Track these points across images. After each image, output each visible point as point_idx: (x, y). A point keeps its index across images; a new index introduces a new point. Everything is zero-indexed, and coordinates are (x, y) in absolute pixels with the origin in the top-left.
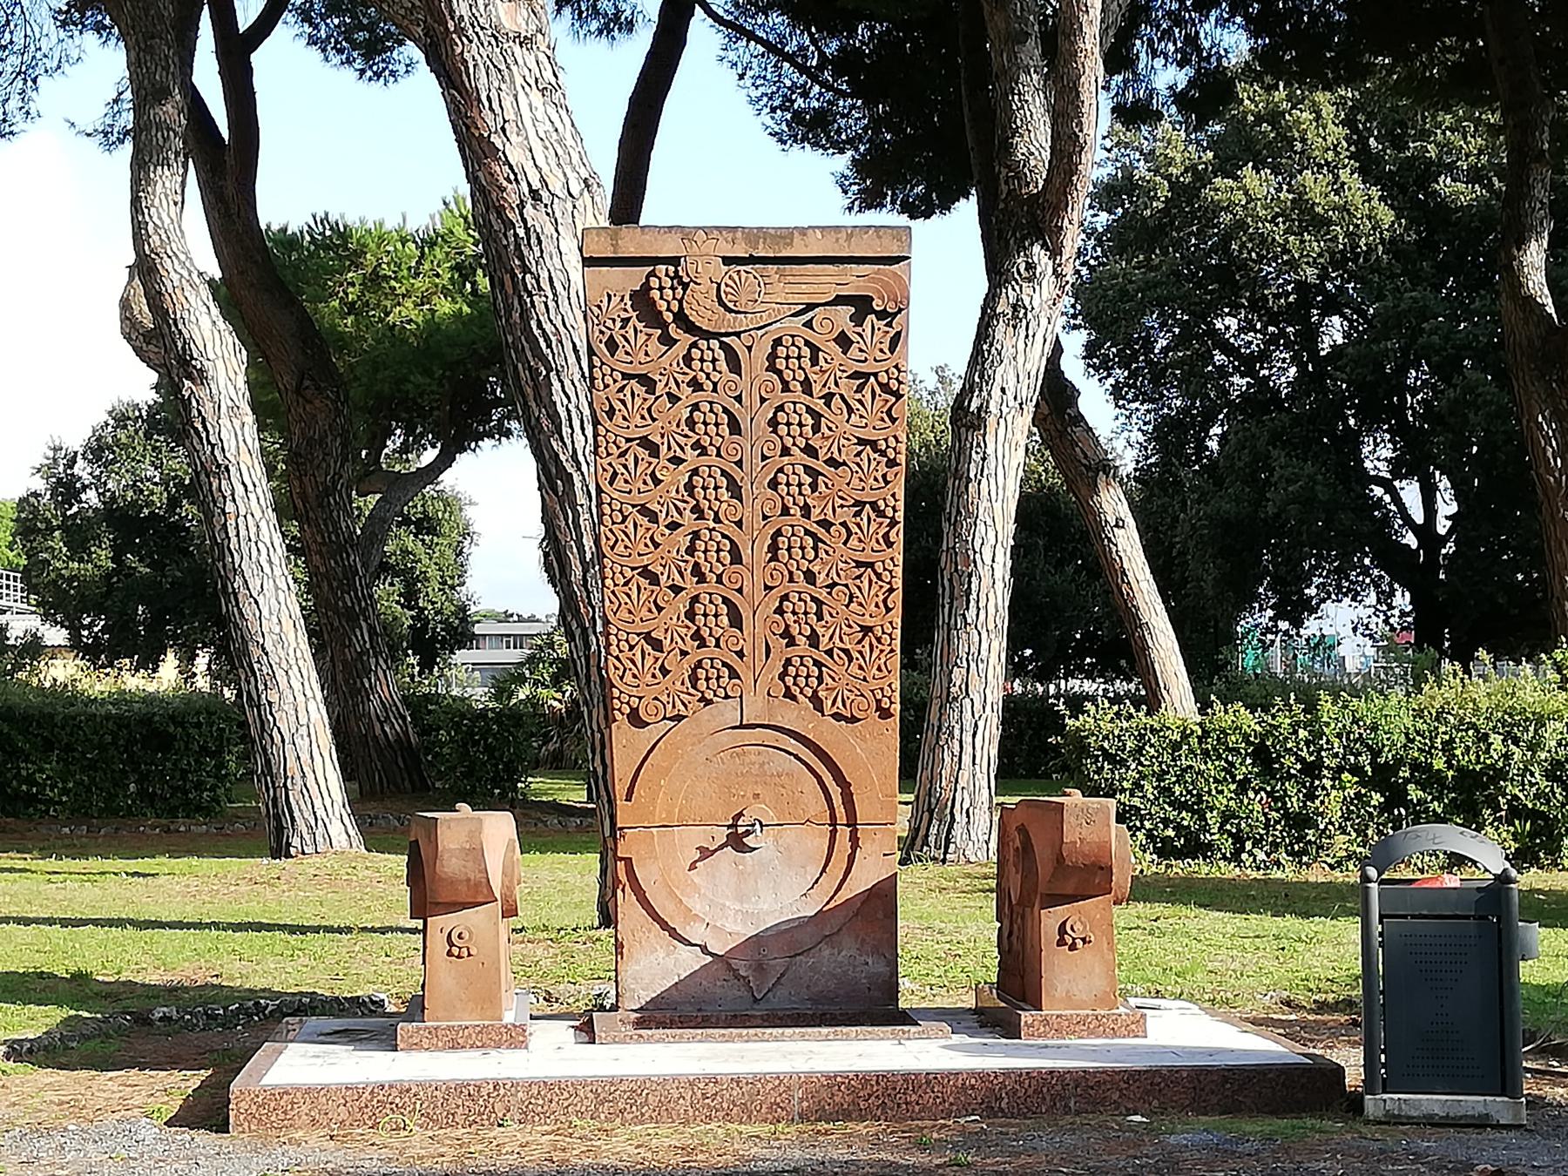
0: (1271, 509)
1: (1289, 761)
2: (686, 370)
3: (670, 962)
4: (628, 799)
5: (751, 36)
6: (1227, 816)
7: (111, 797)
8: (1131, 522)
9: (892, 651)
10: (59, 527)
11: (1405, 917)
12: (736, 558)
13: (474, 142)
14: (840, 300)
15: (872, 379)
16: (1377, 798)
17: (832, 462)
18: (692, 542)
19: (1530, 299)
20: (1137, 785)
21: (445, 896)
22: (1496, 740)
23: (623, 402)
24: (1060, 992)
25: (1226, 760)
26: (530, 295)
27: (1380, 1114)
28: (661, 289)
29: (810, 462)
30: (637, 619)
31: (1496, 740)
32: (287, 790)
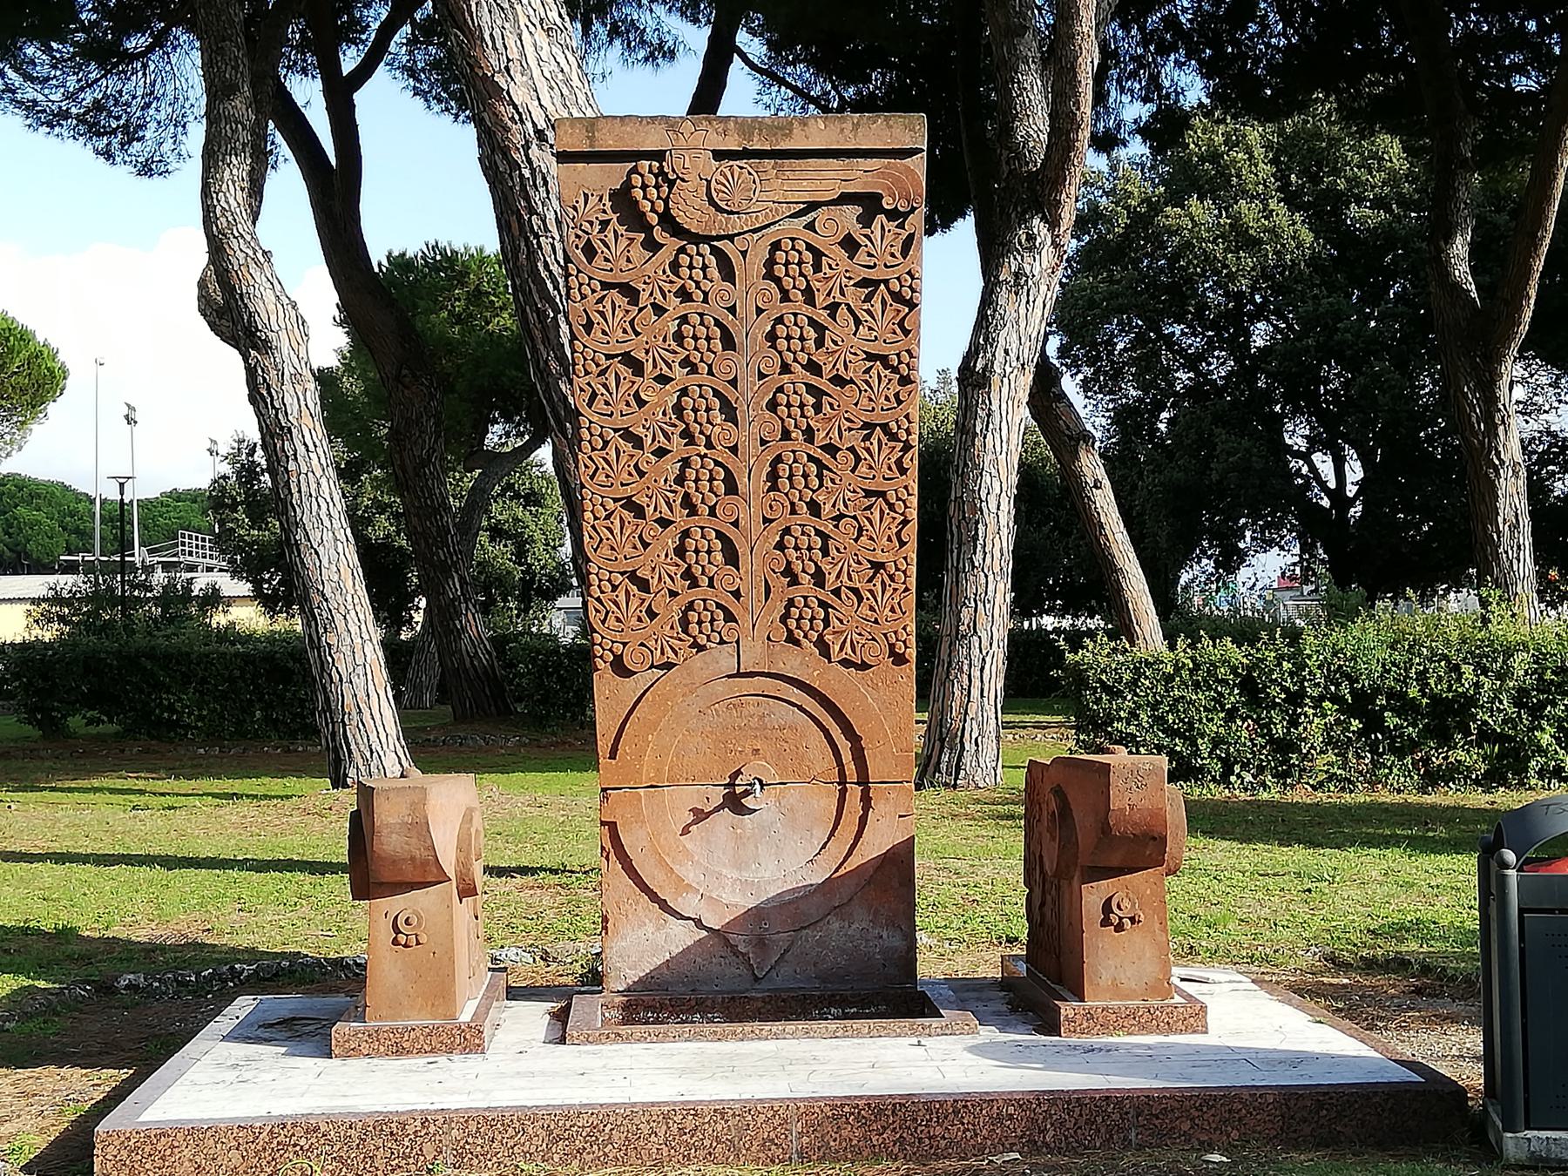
0: (1215, 477)
1: (1274, 691)
2: (675, 279)
4: (613, 756)
5: (782, 82)
6: (1217, 742)
7: (240, 723)
8: (1106, 483)
9: (907, 590)
10: (242, 503)
11: (1551, 911)
12: (731, 488)
14: (845, 199)
16: (1356, 724)
17: (838, 381)
18: (683, 470)
19: (1457, 289)
20: (1133, 714)
21: (387, 875)
23: (602, 314)
24: (1105, 978)
25: (1216, 691)
26: (537, 236)
27: (1523, 1156)
29: (813, 380)
31: (1467, 670)
32: (344, 725)
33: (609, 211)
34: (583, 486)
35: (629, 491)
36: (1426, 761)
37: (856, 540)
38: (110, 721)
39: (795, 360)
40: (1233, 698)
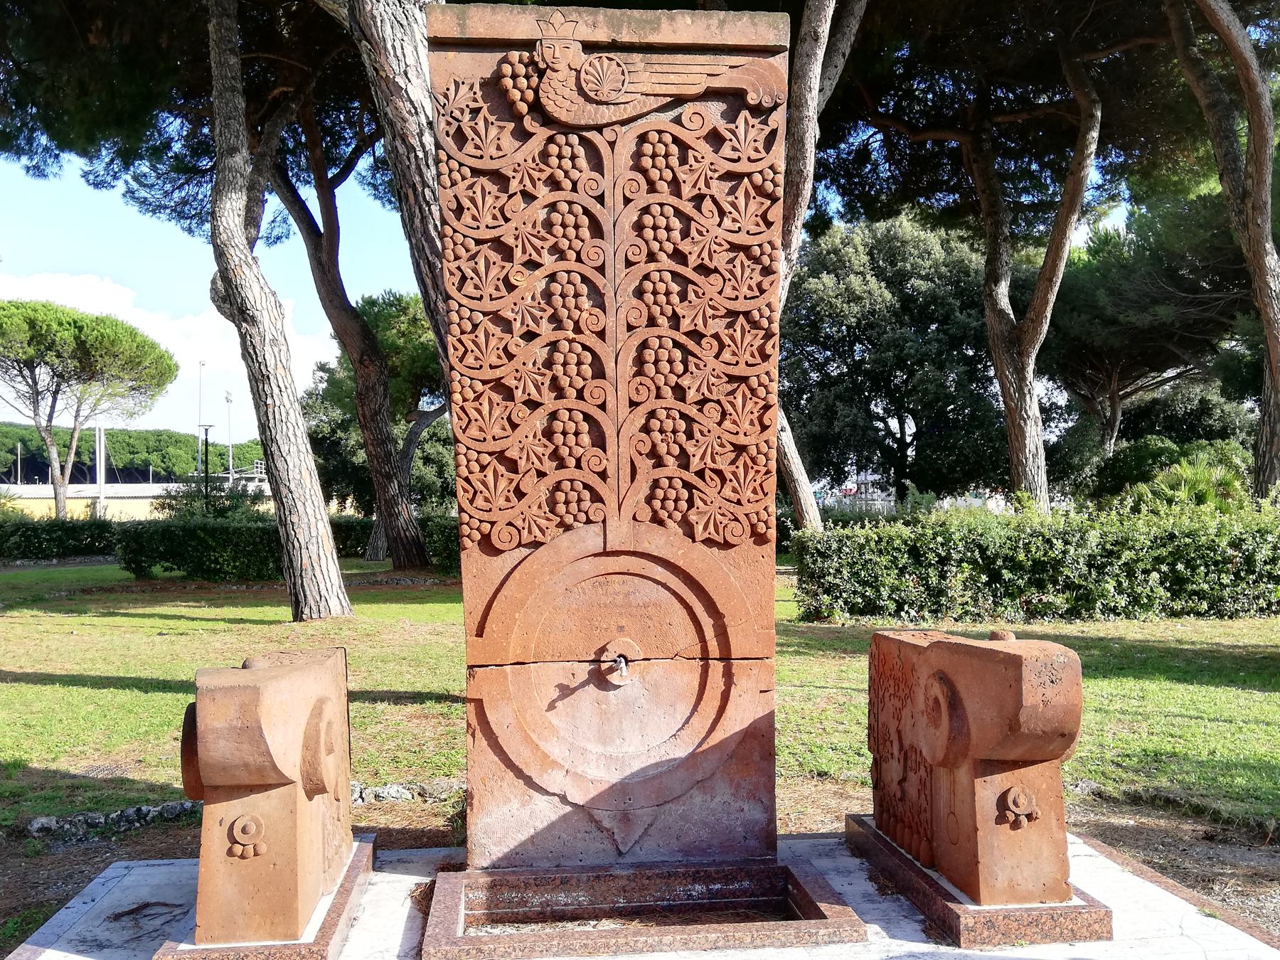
0: (837, 430)
1: (931, 556)
2: (543, 167)
3: (525, 813)
6: (894, 589)
9: (768, 472)
12: (599, 373)
13: (383, 84)
14: (710, 94)
15: (746, 180)
16: (984, 578)
17: (703, 270)
18: (551, 354)
19: (1002, 311)
20: (838, 571)
21: (219, 780)
22: (1059, 544)
24: (1001, 881)
26: (428, 204)
28: (514, 76)
29: (680, 269)
30: (489, 437)
31: (1059, 544)
33: (480, 100)
34: (452, 368)
35: (498, 373)
36: (1028, 602)
37: (719, 424)
39: (661, 249)
40: (904, 560)
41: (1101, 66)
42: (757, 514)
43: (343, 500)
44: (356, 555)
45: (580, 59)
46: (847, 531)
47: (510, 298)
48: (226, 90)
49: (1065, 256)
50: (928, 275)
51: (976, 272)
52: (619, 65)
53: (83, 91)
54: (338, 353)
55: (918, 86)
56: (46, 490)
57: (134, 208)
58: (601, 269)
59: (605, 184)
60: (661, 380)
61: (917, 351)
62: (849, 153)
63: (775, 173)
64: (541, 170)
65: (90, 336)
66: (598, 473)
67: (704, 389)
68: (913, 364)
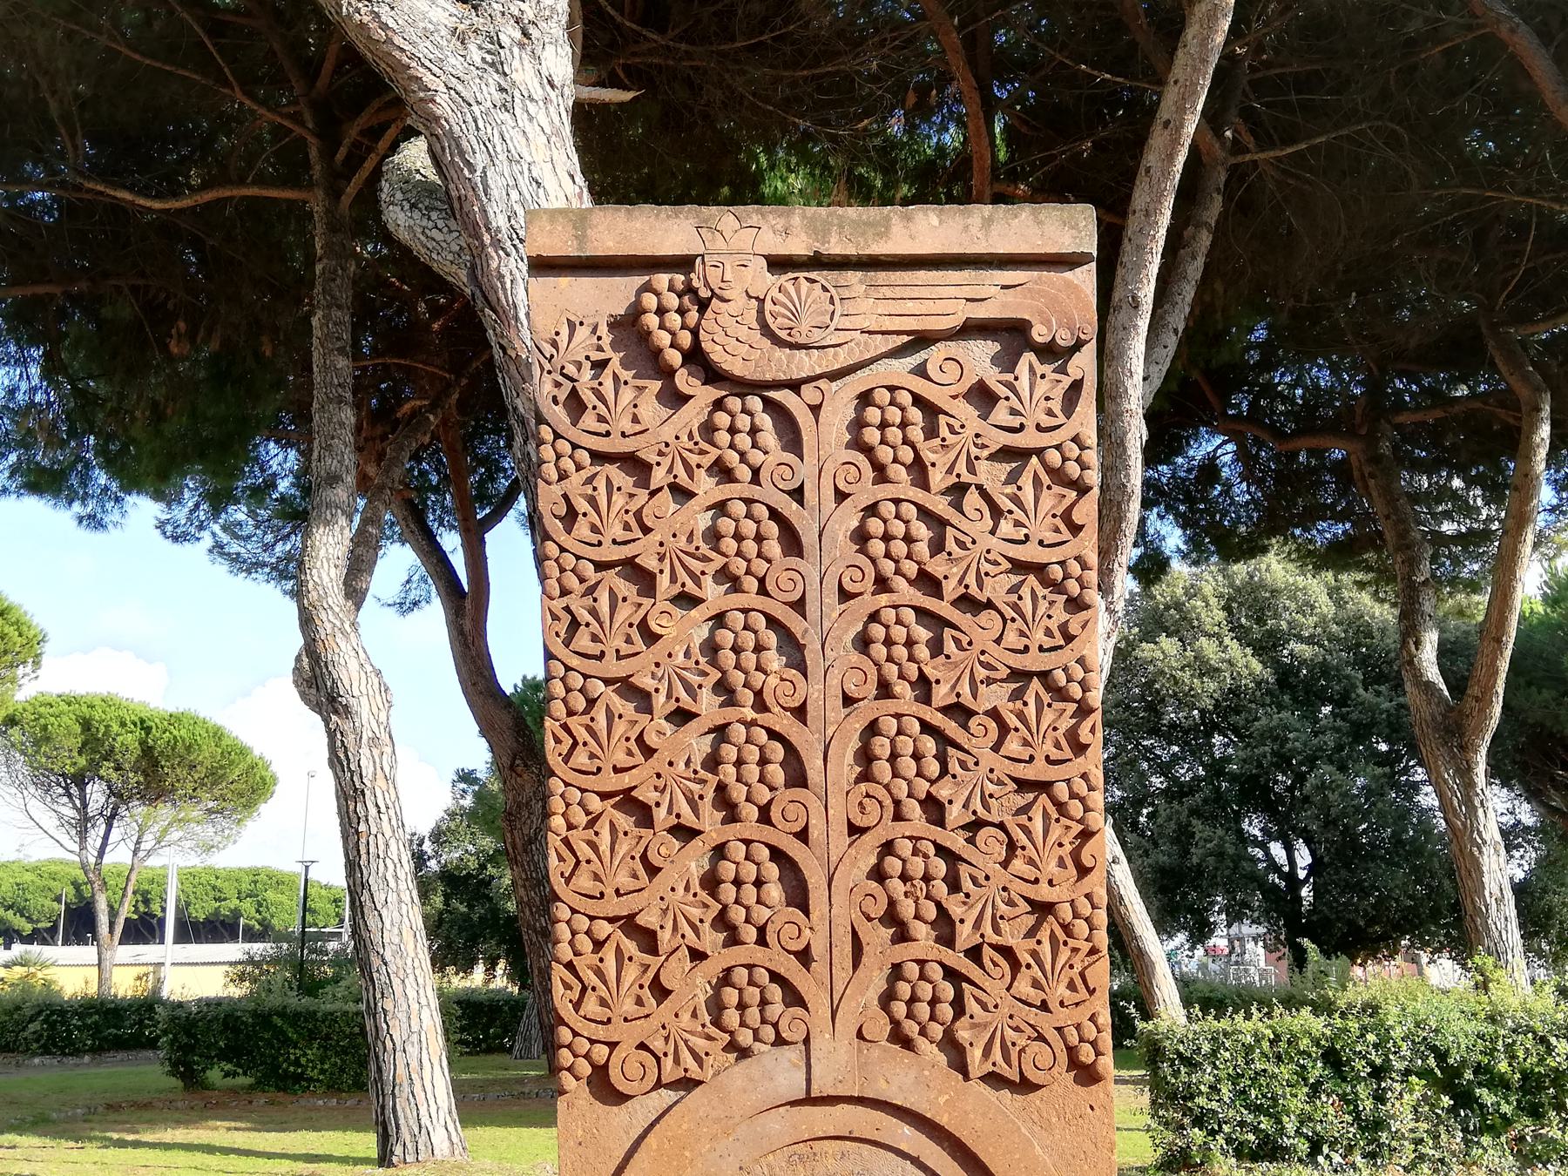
0: (1195, 860)
1: (1359, 1064)
2: (706, 446)
6: (1304, 1119)
9: (1093, 951)
12: (797, 778)
13: (513, 367)
14: (972, 329)
15: (1034, 460)
17: (966, 602)
19: (1429, 686)
28: (661, 311)
29: (930, 603)
30: (610, 891)
33: (607, 348)
35: (626, 780)
36: (1521, 1139)
37: (1005, 864)
38: (245, 1074)
39: (898, 572)
40: (1317, 1070)
41: (1540, 342)
42: (1078, 1027)
43: (491, 965)
44: (502, 1049)
45: (767, 282)
46: (1224, 1024)
47: (650, 655)
48: (331, 401)
49: (1517, 604)
50: (1312, 636)
51: (1383, 631)
52: (825, 289)
53: (158, 415)
54: (488, 756)
55: (1281, 379)
56: (88, 953)
57: (222, 568)
58: (799, 606)
59: (806, 471)
60: (901, 789)
61: (1305, 745)
62: (1189, 471)
63: (1082, 448)
64: (702, 452)
65: (160, 740)
66: (795, 954)
67: (977, 804)
68: (1301, 764)
